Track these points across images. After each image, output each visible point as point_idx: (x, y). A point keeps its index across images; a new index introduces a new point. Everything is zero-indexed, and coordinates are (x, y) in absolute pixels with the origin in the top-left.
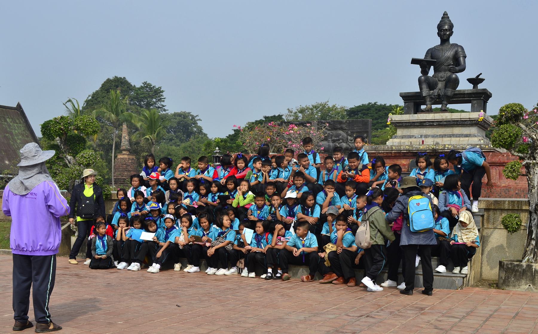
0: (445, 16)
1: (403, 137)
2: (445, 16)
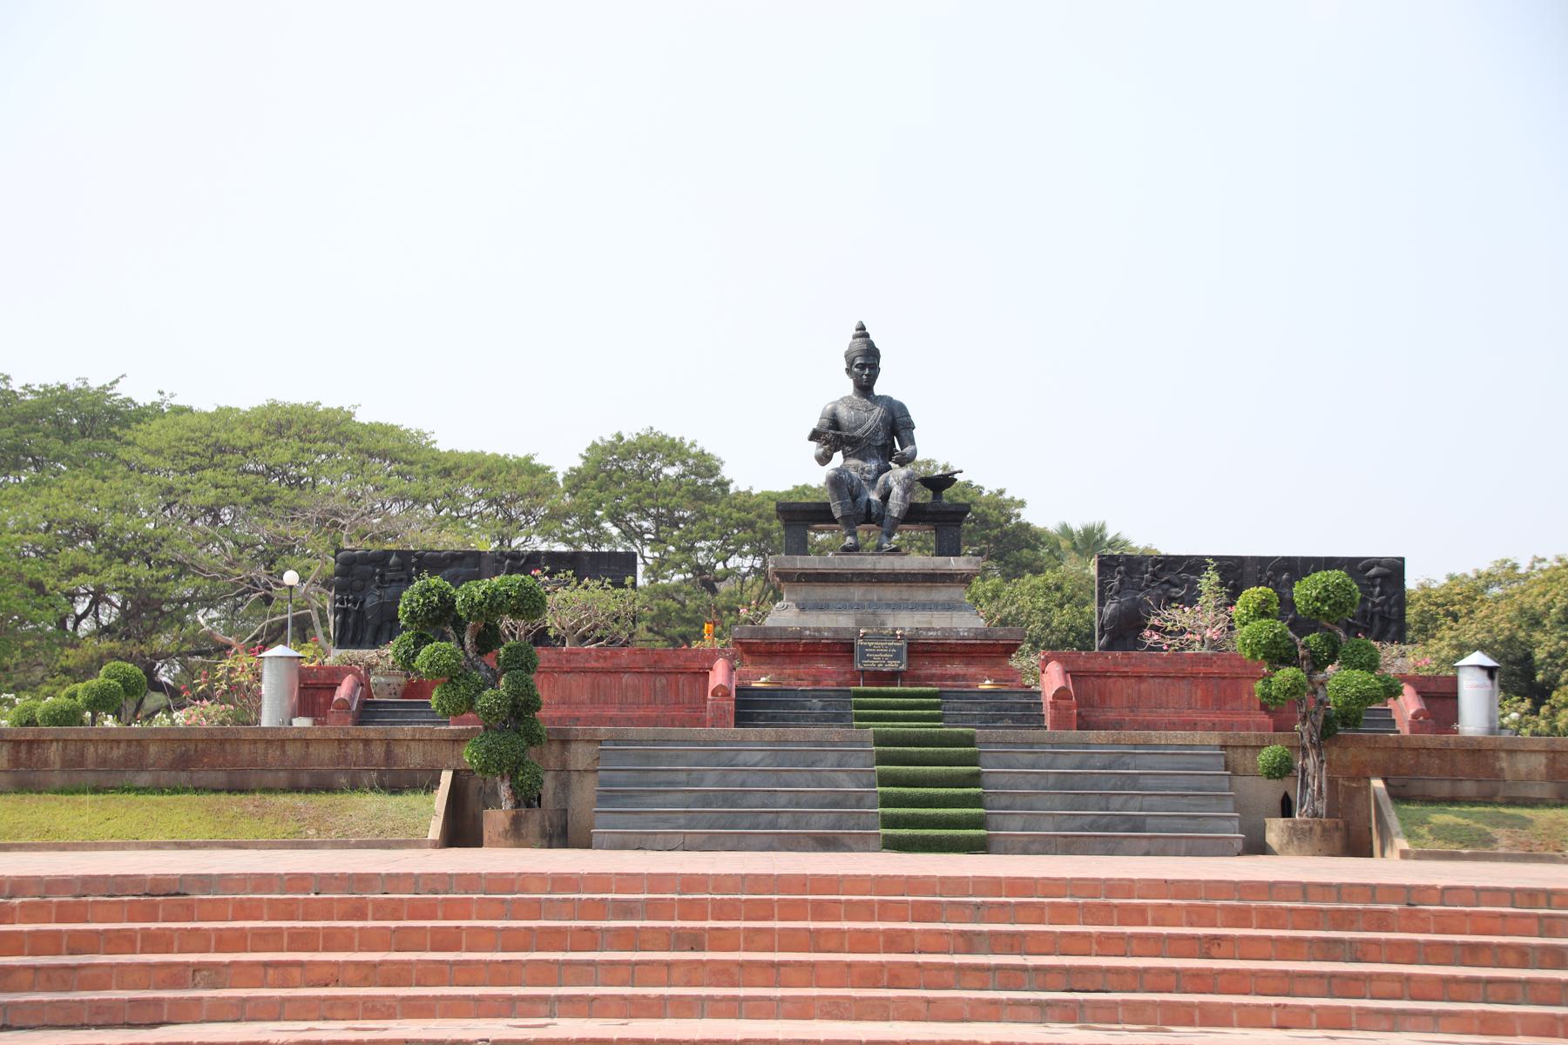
2: (862, 332)
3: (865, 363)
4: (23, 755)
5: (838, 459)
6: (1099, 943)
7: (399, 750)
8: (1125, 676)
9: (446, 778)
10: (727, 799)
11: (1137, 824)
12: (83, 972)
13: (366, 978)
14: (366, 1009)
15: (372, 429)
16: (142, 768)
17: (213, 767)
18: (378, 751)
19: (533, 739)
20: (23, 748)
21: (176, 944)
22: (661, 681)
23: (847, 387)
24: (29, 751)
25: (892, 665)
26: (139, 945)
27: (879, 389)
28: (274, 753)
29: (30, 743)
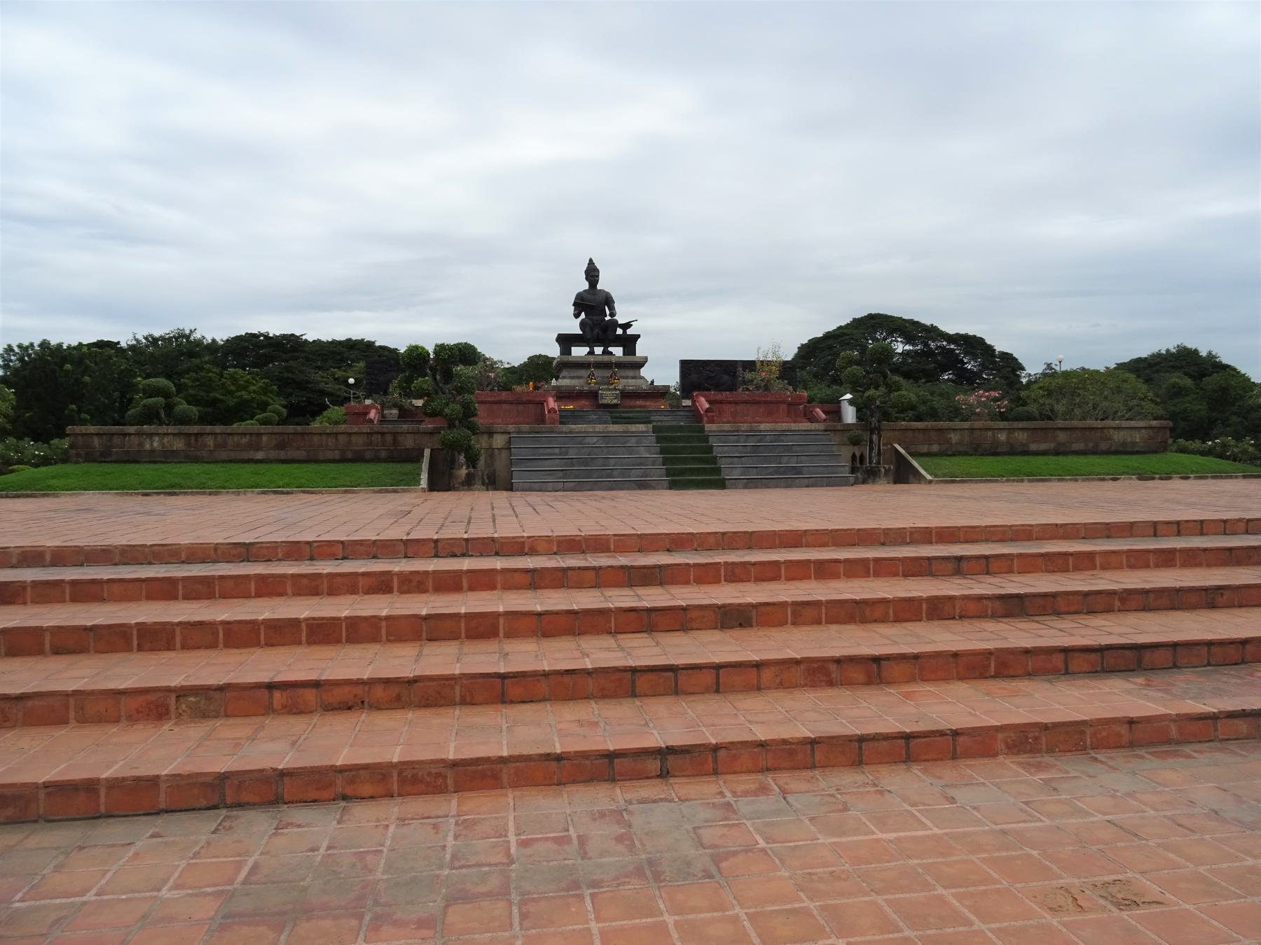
0: (591, 260)
2: (591, 260)
3: (592, 273)
4: (193, 441)
5: (583, 316)
6: (1123, 600)
7: (400, 438)
8: (730, 402)
9: (427, 452)
10: (585, 462)
11: (797, 471)
12: (30, 703)
13: (398, 698)
14: (403, 781)
15: (381, 347)
16: (258, 449)
17: (298, 449)
18: (389, 438)
19: (474, 429)
20: (193, 438)
21: (178, 639)
22: (521, 407)
23: (586, 286)
24: (196, 440)
25: (615, 401)
26: (135, 643)
27: (599, 287)
28: (331, 441)
29: (196, 435)
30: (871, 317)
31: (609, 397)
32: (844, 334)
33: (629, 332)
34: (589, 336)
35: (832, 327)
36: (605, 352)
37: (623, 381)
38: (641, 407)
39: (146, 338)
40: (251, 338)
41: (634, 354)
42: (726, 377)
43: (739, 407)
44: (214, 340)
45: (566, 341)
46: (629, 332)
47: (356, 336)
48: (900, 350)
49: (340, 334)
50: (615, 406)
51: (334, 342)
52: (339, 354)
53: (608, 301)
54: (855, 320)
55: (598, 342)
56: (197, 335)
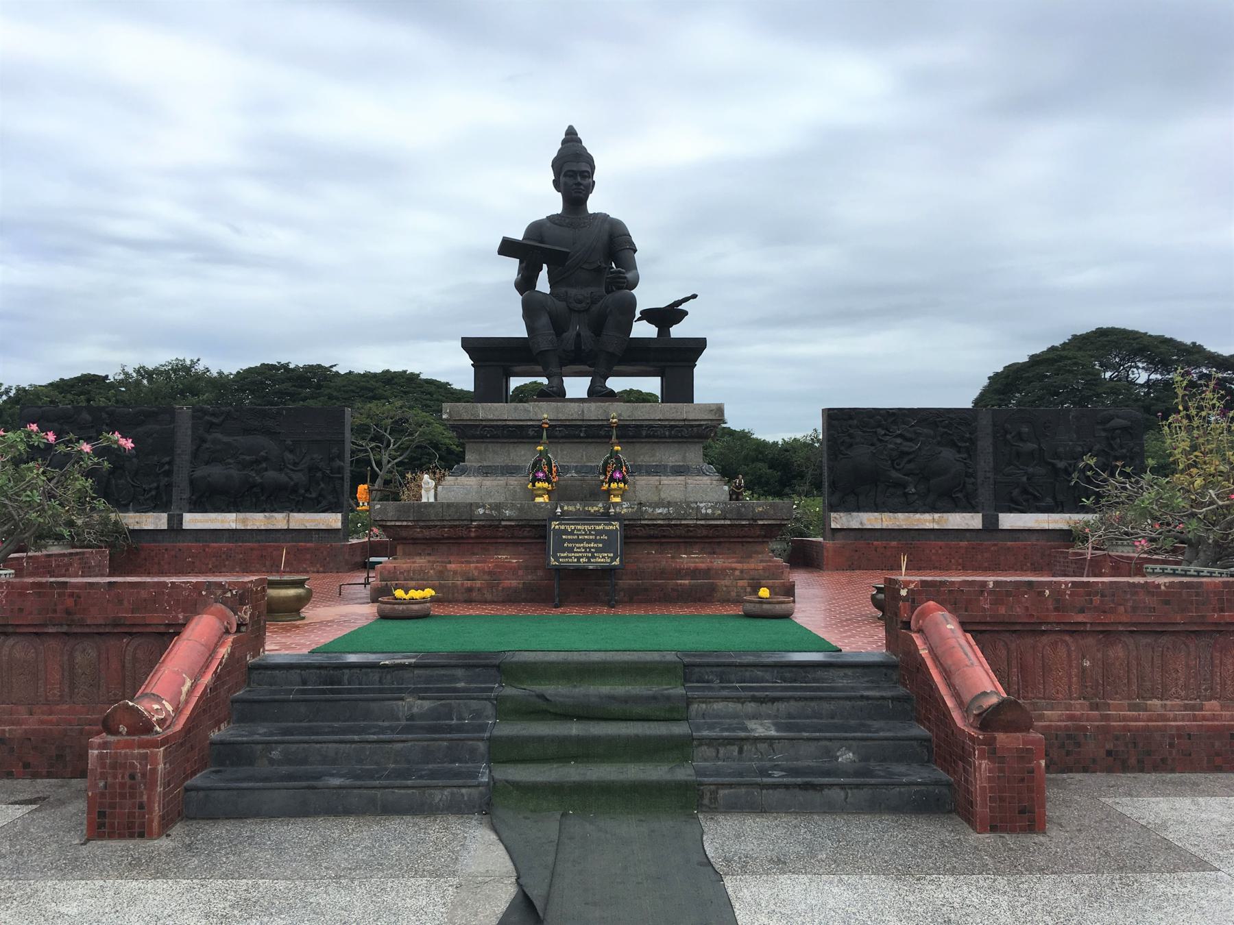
0: (571, 137)
1: (486, 471)
2: (571, 137)
3: (573, 169)
22: (86, 654)
23: (554, 204)
25: (603, 559)
30: (1102, 333)
31: (584, 546)
32: (1062, 358)
33: (677, 331)
34: (545, 342)
35: (1039, 348)
36: (598, 393)
37: (644, 485)
38: (694, 573)
39: (138, 372)
40: (267, 371)
41: (688, 396)
42: (947, 454)
43: (1117, 652)
44: (220, 373)
45: (484, 352)
46: (677, 331)
47: (396, 368)
48: (1142, 380)
49: (377, 367)
50: (607, 572)
51: (368, 376)
52: (372, 390)
53: (615, 245)
54: (1075, 337)
55: (577, 360)
56: (200, 367)
